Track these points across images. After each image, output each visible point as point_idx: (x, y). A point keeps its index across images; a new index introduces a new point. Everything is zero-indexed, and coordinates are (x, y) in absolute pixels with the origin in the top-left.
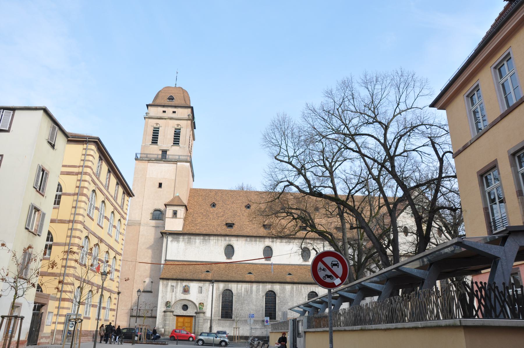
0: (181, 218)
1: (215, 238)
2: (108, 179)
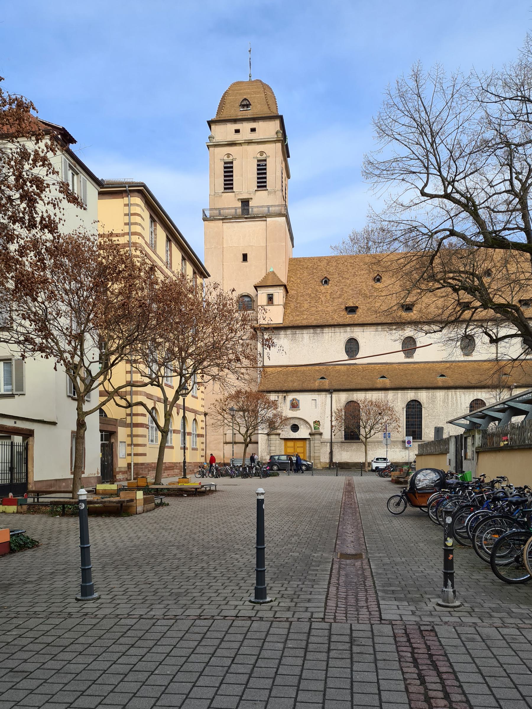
0: (280, 305)
1: (330, 329)
2: (169, 252)
